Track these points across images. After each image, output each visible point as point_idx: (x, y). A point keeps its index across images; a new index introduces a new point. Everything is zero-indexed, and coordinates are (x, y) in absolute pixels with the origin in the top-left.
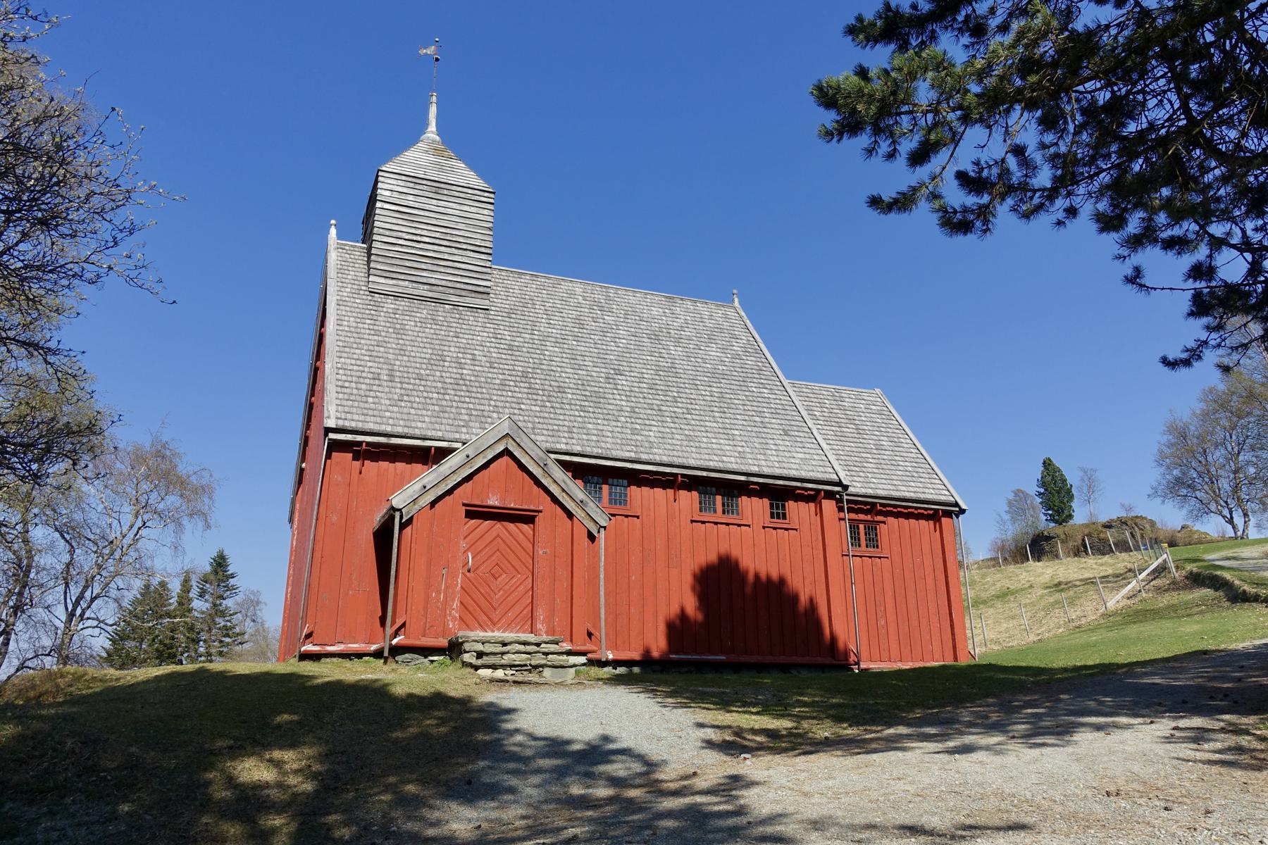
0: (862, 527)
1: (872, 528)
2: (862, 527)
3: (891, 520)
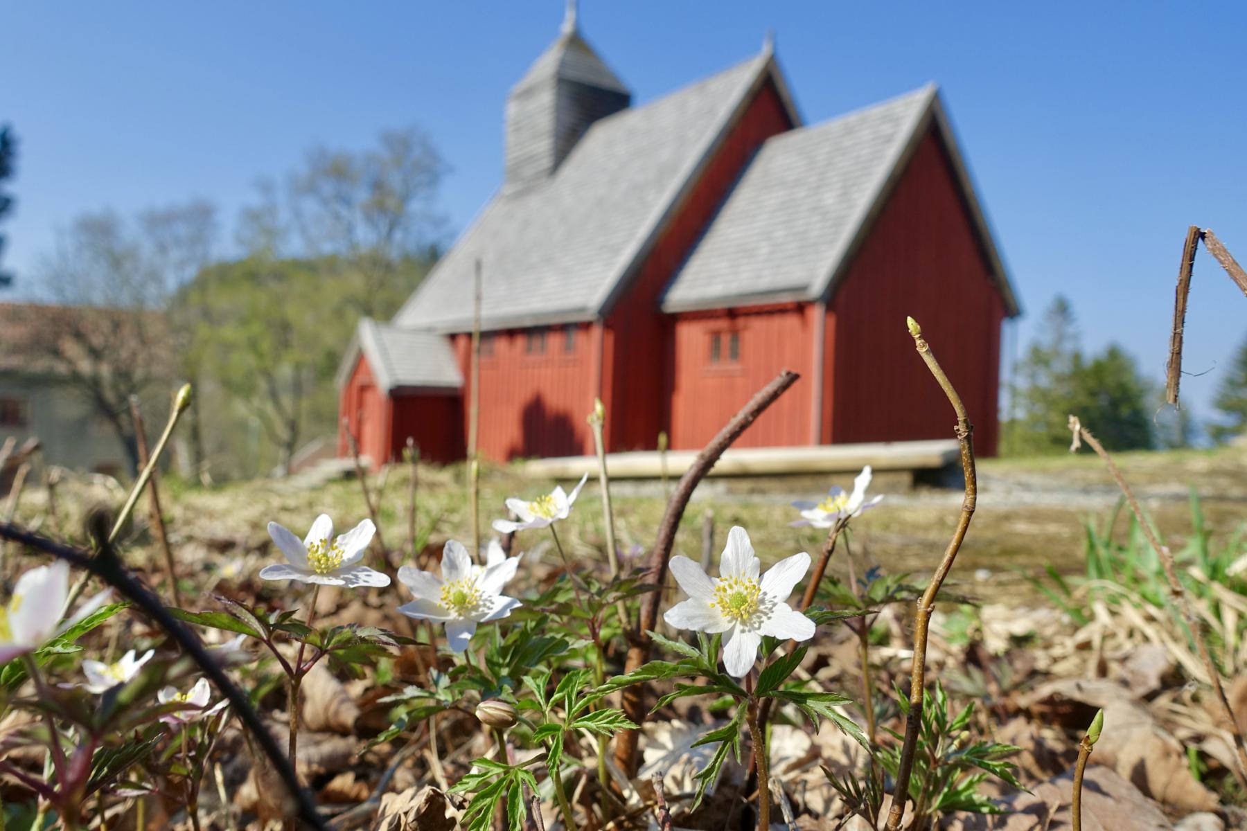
1: (735, 333)
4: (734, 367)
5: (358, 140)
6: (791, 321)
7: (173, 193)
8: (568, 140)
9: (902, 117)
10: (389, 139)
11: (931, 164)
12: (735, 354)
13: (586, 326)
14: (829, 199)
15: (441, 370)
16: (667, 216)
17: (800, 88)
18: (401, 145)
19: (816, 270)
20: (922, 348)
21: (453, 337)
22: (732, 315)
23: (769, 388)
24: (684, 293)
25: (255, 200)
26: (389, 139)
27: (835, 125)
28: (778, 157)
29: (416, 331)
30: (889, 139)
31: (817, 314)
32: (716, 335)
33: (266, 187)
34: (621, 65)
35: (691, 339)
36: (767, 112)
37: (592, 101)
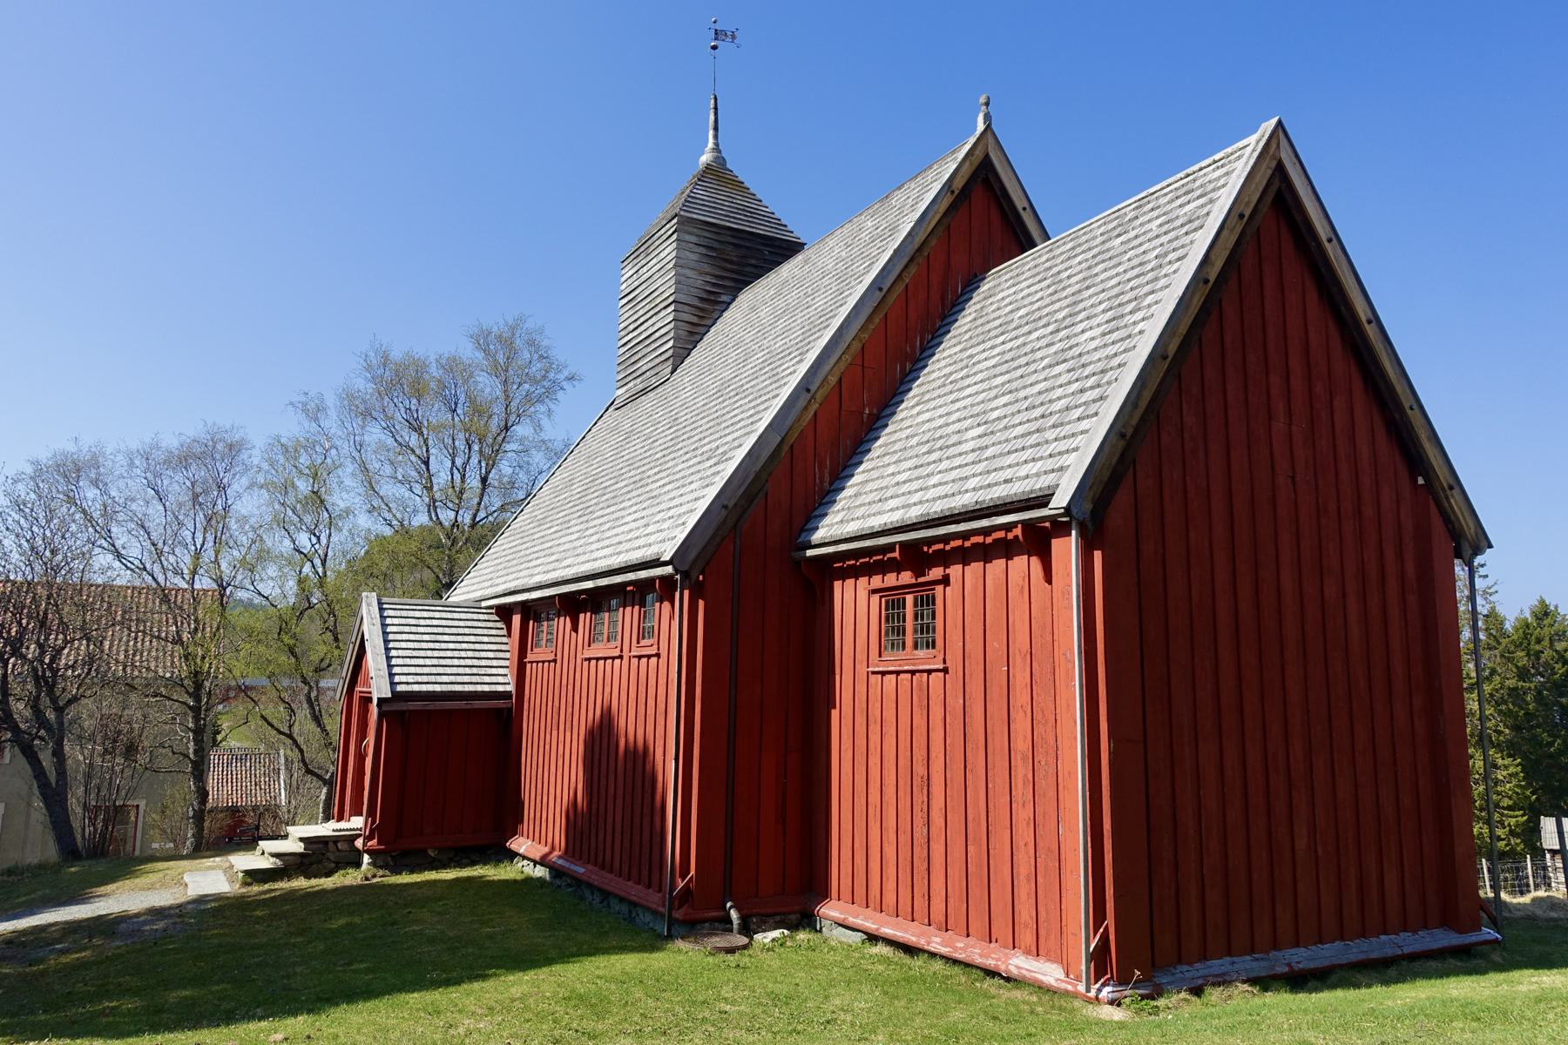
0: (909, 599)
2: (909, 599)
3: (955, 571)
4: (924, 658)
5: (439, 337)
8: (699, 314)
9: (1224, 179)
10: (482, 340)
11: (1279, 297)
12: (926, 639)
13: (666, 588)
14: (1088, 338)
16: (804, 386)
17: (1034, 177)
18: (504, 351)
20: (328, 883)
21: (504, 613)
22: (918, 557)
23: (712, 117)
24: (846, 519)
26: (482, 340)
27: (1097, 225)
28: (1007, 290)
29: (475, 606)
30: (1194, 223)
31: (1067, 549)
33: (314, 412)
34: (780, 200)
35: (855, 605)
36: (983, 223)
37: (735, 252)
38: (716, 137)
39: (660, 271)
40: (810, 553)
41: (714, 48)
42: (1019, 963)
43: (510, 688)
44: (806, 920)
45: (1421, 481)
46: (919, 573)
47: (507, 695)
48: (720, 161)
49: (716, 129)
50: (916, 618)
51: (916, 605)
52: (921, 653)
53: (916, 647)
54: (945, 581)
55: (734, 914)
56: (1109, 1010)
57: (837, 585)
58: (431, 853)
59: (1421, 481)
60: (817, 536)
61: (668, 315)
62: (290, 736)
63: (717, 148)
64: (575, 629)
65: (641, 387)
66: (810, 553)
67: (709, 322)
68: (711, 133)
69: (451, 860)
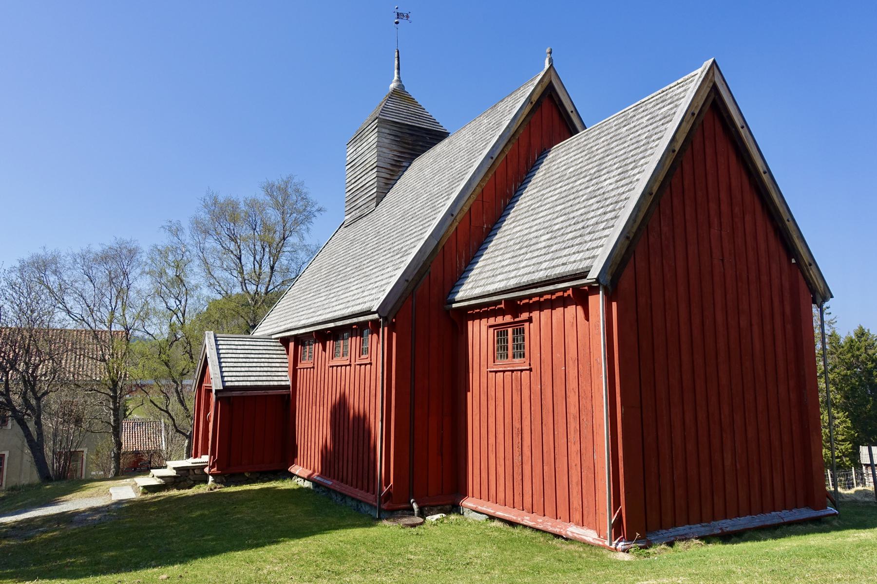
0: (510, 330)
2: (510, 330)
3: (535, 314)
4: (519, 363)
5: (245, 190)
6: (573, 311)
7: (100, 241)
8: (391, 173)
9: (685, 92)
11: (714, 137)
13: (374, 327)
15: (275, 372)
17: (577, 95)
19: (594, 257)
21: (285, 341)
22: (515, 306)
23: (396, 62)
24: (474, 287)
25: (164, 240)
26: (270, 189)
27: (613, 120)
28: (562, 157)
29: (268, 338)
31: (597, 302)
32: (501, 331)
33: (176, 231)
34: (435, 108)
35: (480, 333)
36: (550, 119)
37: (411, 139)
38: (399, 73)
39: (369, 150)
40: (454, 306)
41: (397, 23)
42: (572, 530)
43: (289, 383)
44: (455, 508)
45: (793, 261)
46: (515, 316)
47: (287, 387)
48: (401, 87)
49: (399, 69)
50: (514, 341)
51: (513, 333)
52: (517, 360)
53: (514, 357)
54: (530, 320)
55: (415, 506)
56: (622, 555)
57: (470, 323)
58: (247, 475)
59: (793, 261)
60: (458, 297)
61: (373, 174)
62: (167, 412)
63: (399, 80)
64: (324, 349)
65: (359, 214)
66: (454, 306)
67: (396, 178)
68: (396, 71)
69: (258, 478)
